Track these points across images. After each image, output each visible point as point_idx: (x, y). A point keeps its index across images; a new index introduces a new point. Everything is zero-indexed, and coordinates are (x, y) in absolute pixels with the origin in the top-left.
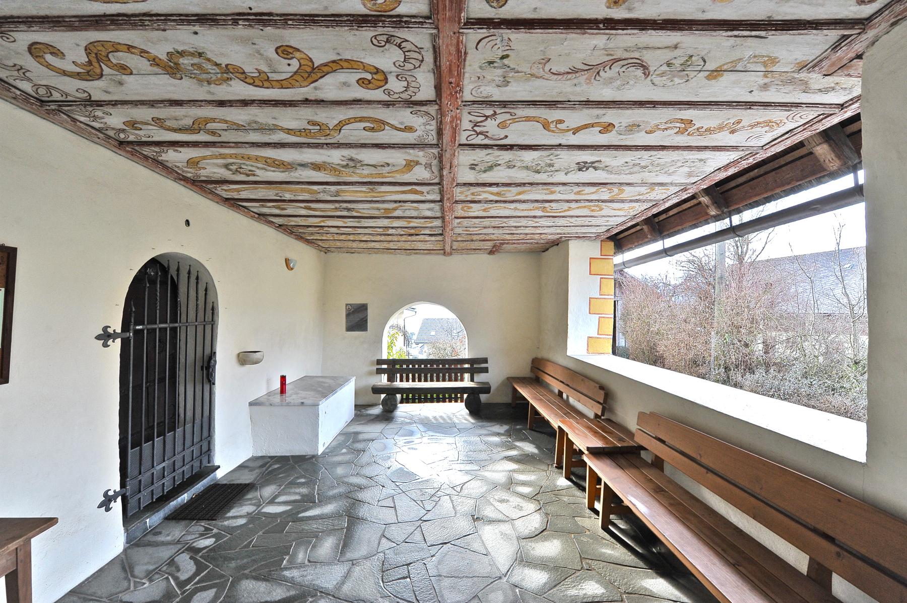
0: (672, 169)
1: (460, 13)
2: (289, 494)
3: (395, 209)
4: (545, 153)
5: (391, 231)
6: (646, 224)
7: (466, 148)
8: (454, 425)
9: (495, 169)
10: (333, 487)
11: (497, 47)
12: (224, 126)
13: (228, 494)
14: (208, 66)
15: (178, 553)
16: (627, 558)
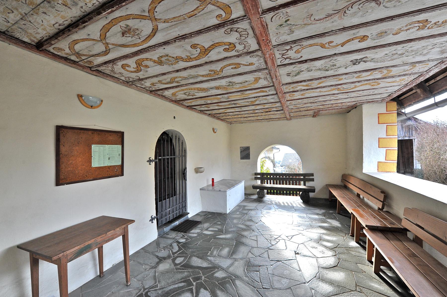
0: (425, 52)
1: (258, 9)
2: (213, 227)
3: (256, 101)
4: (327, 60)
5: (256, 111)
6: (418, 88)
7: (281, 67)
8: (293, 207)
9: (301, 73)
10: (231, 228)
11: (281, 17)
12: (180, 79)
13: (190, 224)
14: (170, 59)
15: (173, 242)
16: (389, 292)
